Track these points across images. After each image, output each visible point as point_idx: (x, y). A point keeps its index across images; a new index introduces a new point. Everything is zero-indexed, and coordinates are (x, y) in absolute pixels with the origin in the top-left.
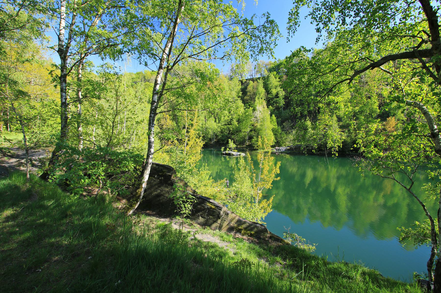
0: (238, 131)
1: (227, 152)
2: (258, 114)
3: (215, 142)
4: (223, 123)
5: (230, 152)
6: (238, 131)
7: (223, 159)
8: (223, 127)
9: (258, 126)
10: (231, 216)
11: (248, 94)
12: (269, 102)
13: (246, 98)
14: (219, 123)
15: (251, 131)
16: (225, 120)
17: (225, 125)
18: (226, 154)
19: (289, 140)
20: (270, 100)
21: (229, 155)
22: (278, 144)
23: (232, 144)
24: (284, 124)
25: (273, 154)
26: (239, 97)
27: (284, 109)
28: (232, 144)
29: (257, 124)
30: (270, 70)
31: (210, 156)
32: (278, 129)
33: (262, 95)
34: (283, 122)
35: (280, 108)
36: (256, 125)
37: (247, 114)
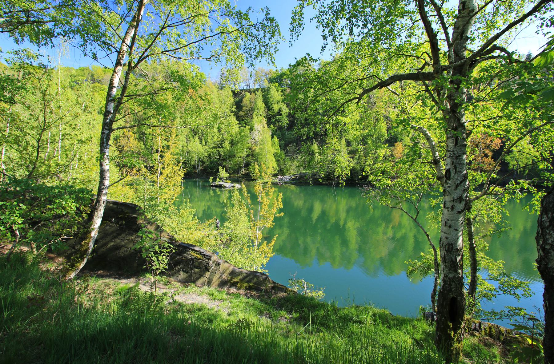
1: (217, 183)
2: (256, 134)
4: (212, 146)
5: (221, 183)
6: (231, 156)
7: (211, 192)
8: (211, 150)
9: (257, 149)
11: (244, 108)
12: (270, 120)
13: (241, 113)
15: (248, 156)
16: (214, 142)
17: (215, 147)
18: (216, 186)
21: (220, 186)
22: (281, 172)
23: (223, 173)
25: (274, 184)
26: (232, 112)
28: (223, 173)
29: (255, 147)
30: (271, 81)
31: (194, 189)
32: (281, 155)
33: (261, 110)
36: (254, 149)
37: (243, 134)
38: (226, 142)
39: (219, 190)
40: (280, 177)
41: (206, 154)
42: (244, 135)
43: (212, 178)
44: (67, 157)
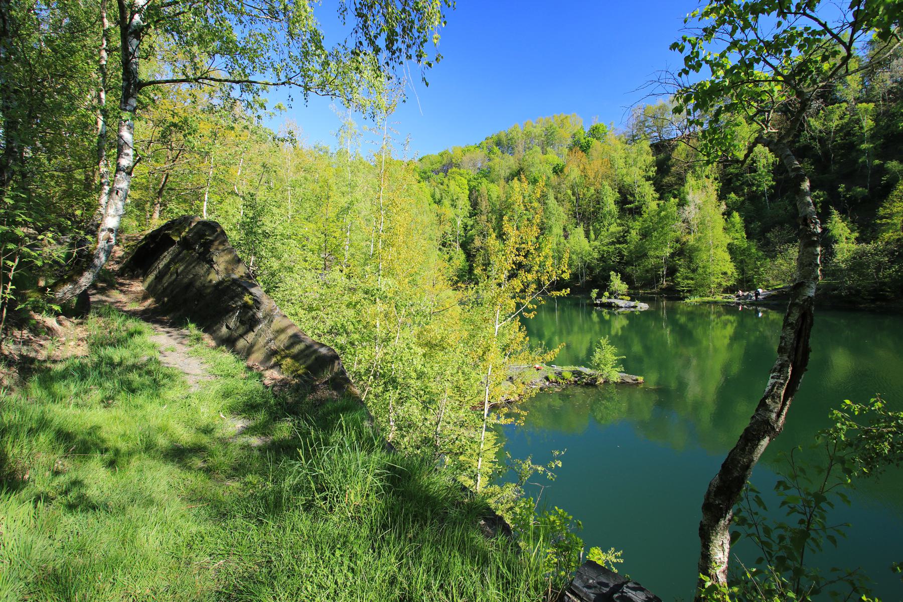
0: (641, 254)
3: (587, 281)
4: (607, 241)
6: (641, 254)
7: (594, 316)
8: (605, 248)
9: (691, 239)
10: (278, 323)
13: (667, 179)
14: (596, 239)
16: (612, 233)
17: (613, 243)
18: (603, 305)
19: (781, 268)
20: (731, 179)
21: (609, 306)
22: (745, 282)
23: (617, 283)
24: (768, 235)
25: (729, 308)
26: (648, 179)
27: (772, 198)
28: (617, 283)
31: (574, 313)
32: (749, 248)
34: (766, 229)
35: (759, 198)
36: (684, 240)
37: (663, 213)
38: (632, 231)
39: (609, 313)
40: (741, 293)
41: (596, 255)
42: (666, 217)
43: (597, 290)
44: (351, 246)
